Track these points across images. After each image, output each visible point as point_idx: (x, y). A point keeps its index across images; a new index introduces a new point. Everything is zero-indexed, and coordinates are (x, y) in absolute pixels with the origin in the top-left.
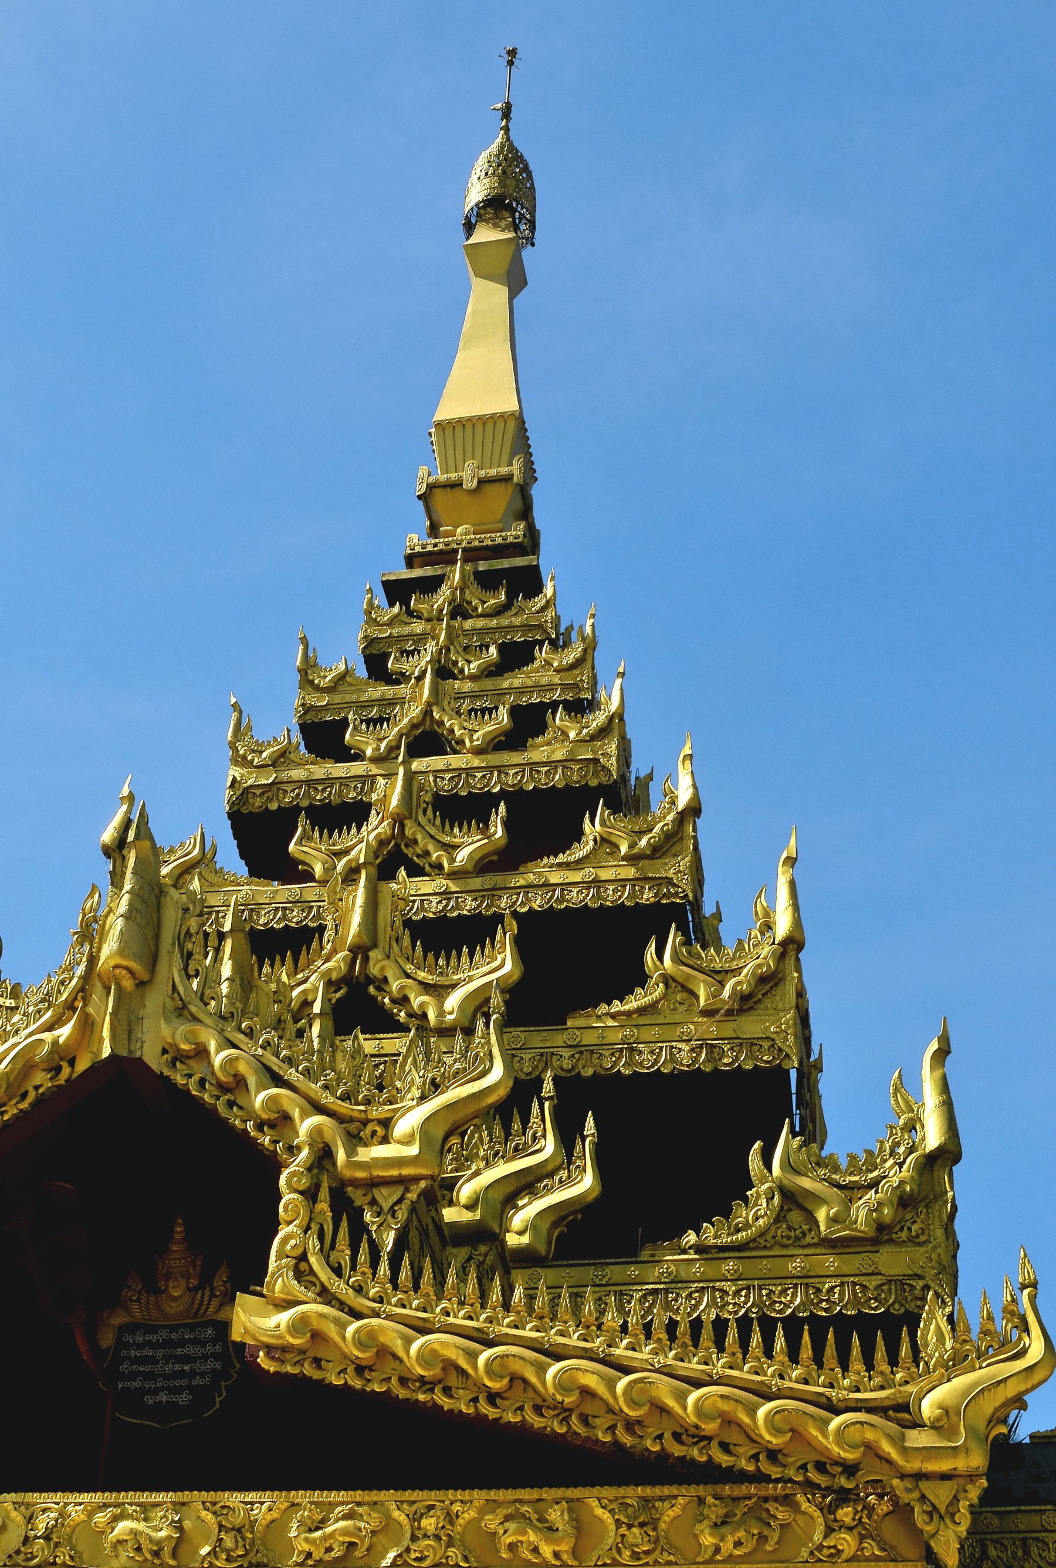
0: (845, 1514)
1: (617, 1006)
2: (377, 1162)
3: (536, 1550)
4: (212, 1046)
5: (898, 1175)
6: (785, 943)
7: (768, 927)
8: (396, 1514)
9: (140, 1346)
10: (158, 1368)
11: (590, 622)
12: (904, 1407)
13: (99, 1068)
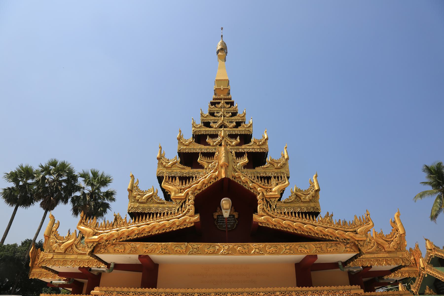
0: (348, 246)
1: (262, 167)
2: (271, 195)
4: (241, 177)
5: (312, 193)
7: (284, 157)
12: (355, 231)
13: (223, 180)
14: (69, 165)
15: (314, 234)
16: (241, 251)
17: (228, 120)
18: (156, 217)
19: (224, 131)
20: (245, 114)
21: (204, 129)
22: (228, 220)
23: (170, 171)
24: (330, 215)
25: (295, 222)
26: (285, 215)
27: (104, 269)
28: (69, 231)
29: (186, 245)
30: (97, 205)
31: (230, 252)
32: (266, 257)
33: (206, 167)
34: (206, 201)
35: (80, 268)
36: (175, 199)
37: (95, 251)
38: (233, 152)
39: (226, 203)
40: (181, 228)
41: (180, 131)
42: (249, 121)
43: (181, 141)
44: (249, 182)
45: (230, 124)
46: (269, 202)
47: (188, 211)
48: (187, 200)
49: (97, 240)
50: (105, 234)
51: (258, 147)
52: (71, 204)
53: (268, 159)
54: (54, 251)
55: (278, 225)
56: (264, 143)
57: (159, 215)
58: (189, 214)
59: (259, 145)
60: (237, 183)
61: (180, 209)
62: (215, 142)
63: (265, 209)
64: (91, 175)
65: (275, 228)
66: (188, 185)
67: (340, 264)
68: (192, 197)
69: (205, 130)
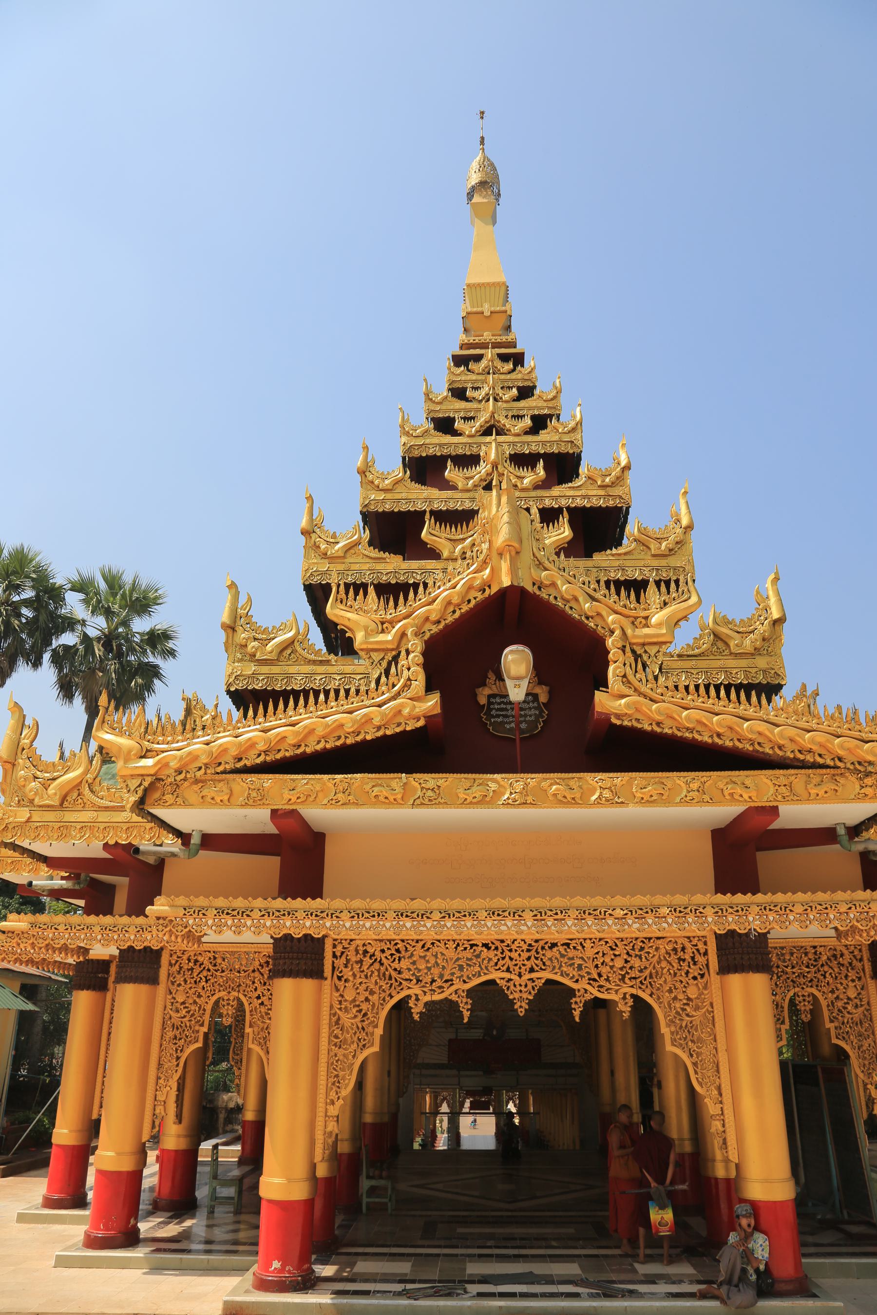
0: (869, 781)
1: (614, 551)
2: (647, 636)
3: (741, 796)
4: (559, 583)
5: (763, 629)
6: (686, 528)
8: (678, 782)
9: (499, 704)
10: (509, 713)
11: (558, 381)
13: (504, 593)
14: (36, 555)
15: (711, 737)
16: (560, 797)
17: (507, 410)
18: (316, 703)
19: (499, 444)
20: (559, 392)
21: (435, 440)
22: (521, 709)
23: (341, 567)
24: (809, 693)
25: (717, 714)
26: (688, 693)
27: (175, 850)
28: (61, 745)
29: (404, 780)
30: (127, 672)
31: (529, 799)
32: (633, 811)
33: (445, 554)
34: (458, 655)
35: (106, 846)
36: (368, 651)
37: (149, 801)
38: (534, 511)
39: (516, 661)
40: (388, 733)
41: (366, 448)
42: (571, 412)
43: (370, 477)
44: (581, 599)
45: (514, 422)
46: (640, 656)
47: (407, 685)
48: (403, 653)
49: (152, 772)
50: (177, 751)
51: (602, 492)
52: (53, 669)
53: (632, 528)
54: (32, 801)
55: (668, 723)
56: (619, 480)
57: (322, 697)
58: (410, 693)
59: (603, 487)
60: (548, 603)
61: (383, 679)
62: (472, 478)
63: (631, 677)
64: (103, 585)
65: (658, 730)
66: (402, 610)
67: (841, 831)
68: (416, 646)
69: (438, 443)
